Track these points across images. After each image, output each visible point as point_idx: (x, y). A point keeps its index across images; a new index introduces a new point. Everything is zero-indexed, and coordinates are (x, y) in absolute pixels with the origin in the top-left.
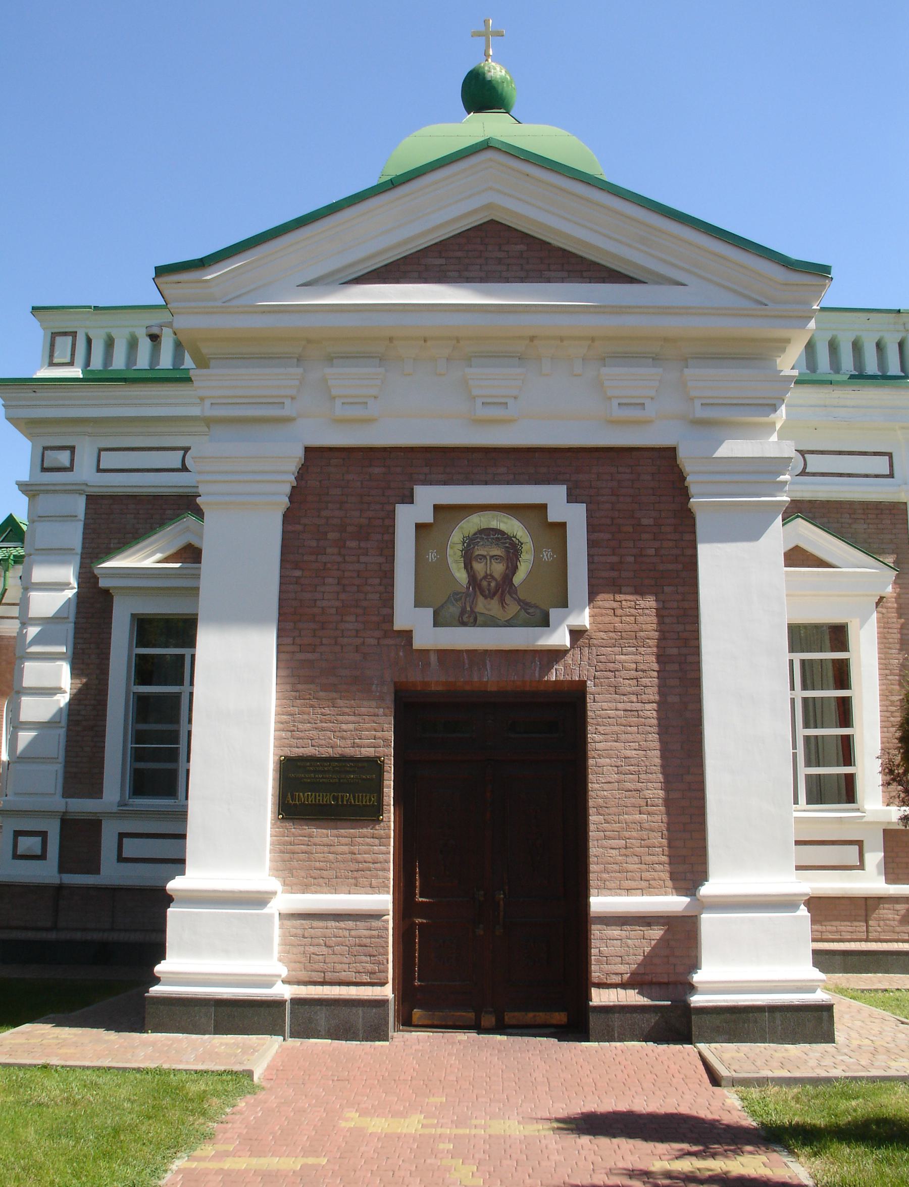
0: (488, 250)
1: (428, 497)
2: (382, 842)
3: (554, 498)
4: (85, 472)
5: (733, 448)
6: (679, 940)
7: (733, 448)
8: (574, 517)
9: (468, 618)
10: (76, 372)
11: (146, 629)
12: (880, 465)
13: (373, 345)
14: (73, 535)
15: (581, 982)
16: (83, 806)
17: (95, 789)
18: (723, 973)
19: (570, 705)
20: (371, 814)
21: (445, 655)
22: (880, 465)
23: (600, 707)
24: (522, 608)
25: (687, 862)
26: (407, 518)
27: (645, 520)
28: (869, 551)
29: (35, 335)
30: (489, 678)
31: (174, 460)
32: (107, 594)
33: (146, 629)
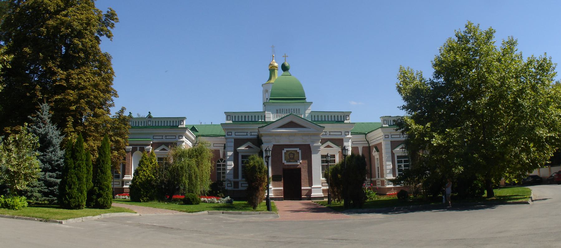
0: (291, 125)
1: (285, 150)
2: (282, 183)
3: (298, 149)
4: (233, 136)
5: (315, 145)
6: (310, 191)
7: (315, 145)
8: (300, 151)
9: (290, 162)
10: (231, 122)
11: (243, 157)
12: (340, 133)
13: (280, 134)
14: (232, 144)
15: (301, 195)
16: (236, 180)
17: (238, 178)
18: (314, 194)
19: (300, 169)
20: (281, 180)
21: (288, 165)
22: (340, 133)
23: (302, 170)
24: (265, 122)
25: (311, 184)
26: (284, 152)
27: (307, 152)
28: (338, 146)
29: (225, 116)
30: (292, 167)
31: (245, 134)
32: (238, 153)
33: (243, 157)
